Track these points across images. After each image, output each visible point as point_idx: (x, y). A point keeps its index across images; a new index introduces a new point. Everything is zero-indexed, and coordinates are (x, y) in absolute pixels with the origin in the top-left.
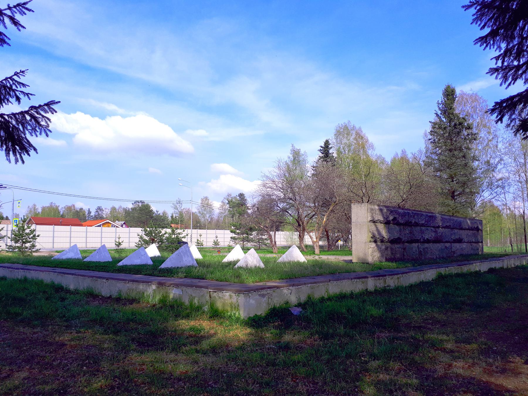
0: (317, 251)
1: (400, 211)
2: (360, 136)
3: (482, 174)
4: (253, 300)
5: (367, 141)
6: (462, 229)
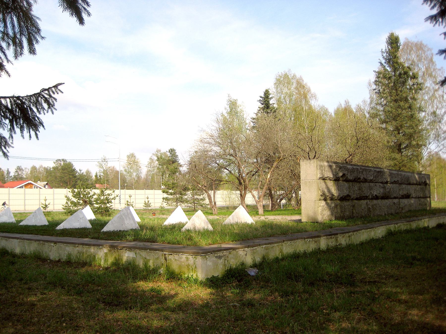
0: (261, 211)
1: (349, 167)
2: (300, 85)
3: (428, 125)
4: (211, 261)
5: (309, 91)
6: (410, 184)
